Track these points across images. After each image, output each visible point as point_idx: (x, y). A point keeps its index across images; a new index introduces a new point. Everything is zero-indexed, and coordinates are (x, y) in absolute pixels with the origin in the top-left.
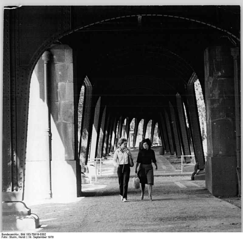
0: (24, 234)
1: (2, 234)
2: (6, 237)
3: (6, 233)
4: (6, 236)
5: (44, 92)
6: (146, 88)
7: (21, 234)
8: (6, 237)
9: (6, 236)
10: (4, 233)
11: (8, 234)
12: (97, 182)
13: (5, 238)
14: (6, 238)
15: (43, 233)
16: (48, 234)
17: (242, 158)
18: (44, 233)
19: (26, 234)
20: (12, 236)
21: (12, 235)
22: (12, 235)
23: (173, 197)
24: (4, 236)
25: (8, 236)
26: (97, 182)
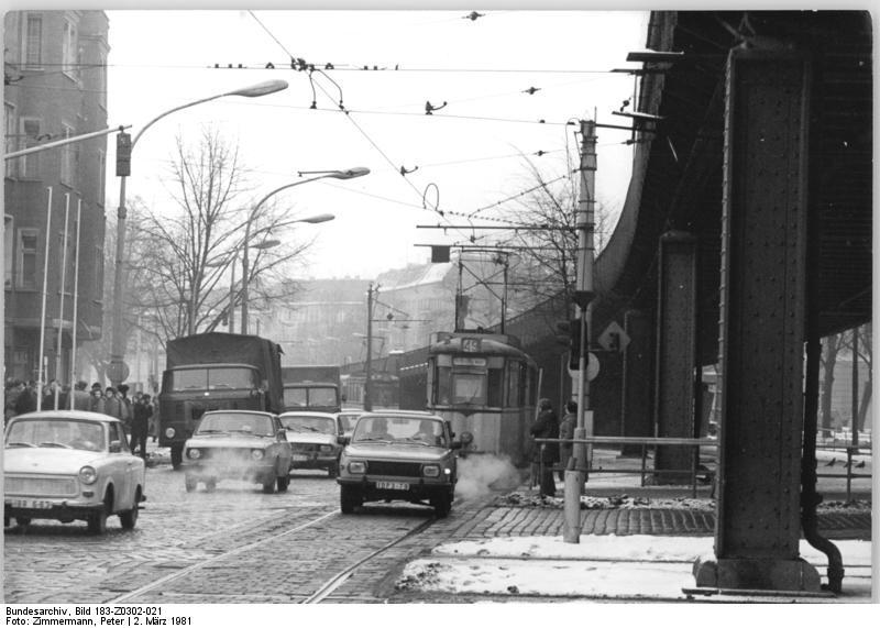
0: (88, 612)
1: (8, 611)
2: (23, 622)
3: (22, 607)
4: (21, 617)
5: (734, 195)
6: (713, 408)
7: (78, 611)
8: (23, 622)
9: (21, 617)
10: (14, 607)
11: (31, 612)
12: (438, 341)
13: (17, 626)
14: (21, 626)
15: (131, 606)
16: (170, 610)
17: (530, 604)
18: (137, 606)
19: (93, 611)
20: (43, 617)
21: (43, 612)
22: (43, 612)
23: (528, 577)
24: (15, 617)
25: (30, 618)
26: (438, 341)
